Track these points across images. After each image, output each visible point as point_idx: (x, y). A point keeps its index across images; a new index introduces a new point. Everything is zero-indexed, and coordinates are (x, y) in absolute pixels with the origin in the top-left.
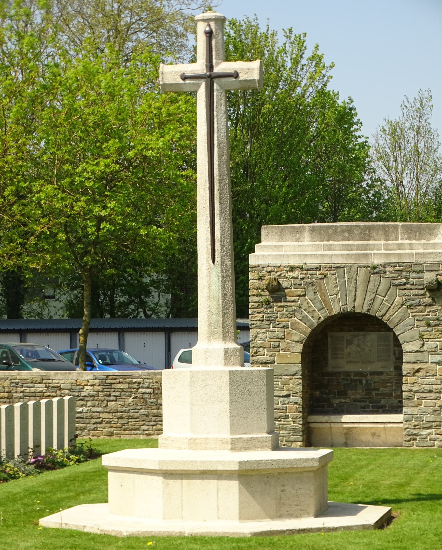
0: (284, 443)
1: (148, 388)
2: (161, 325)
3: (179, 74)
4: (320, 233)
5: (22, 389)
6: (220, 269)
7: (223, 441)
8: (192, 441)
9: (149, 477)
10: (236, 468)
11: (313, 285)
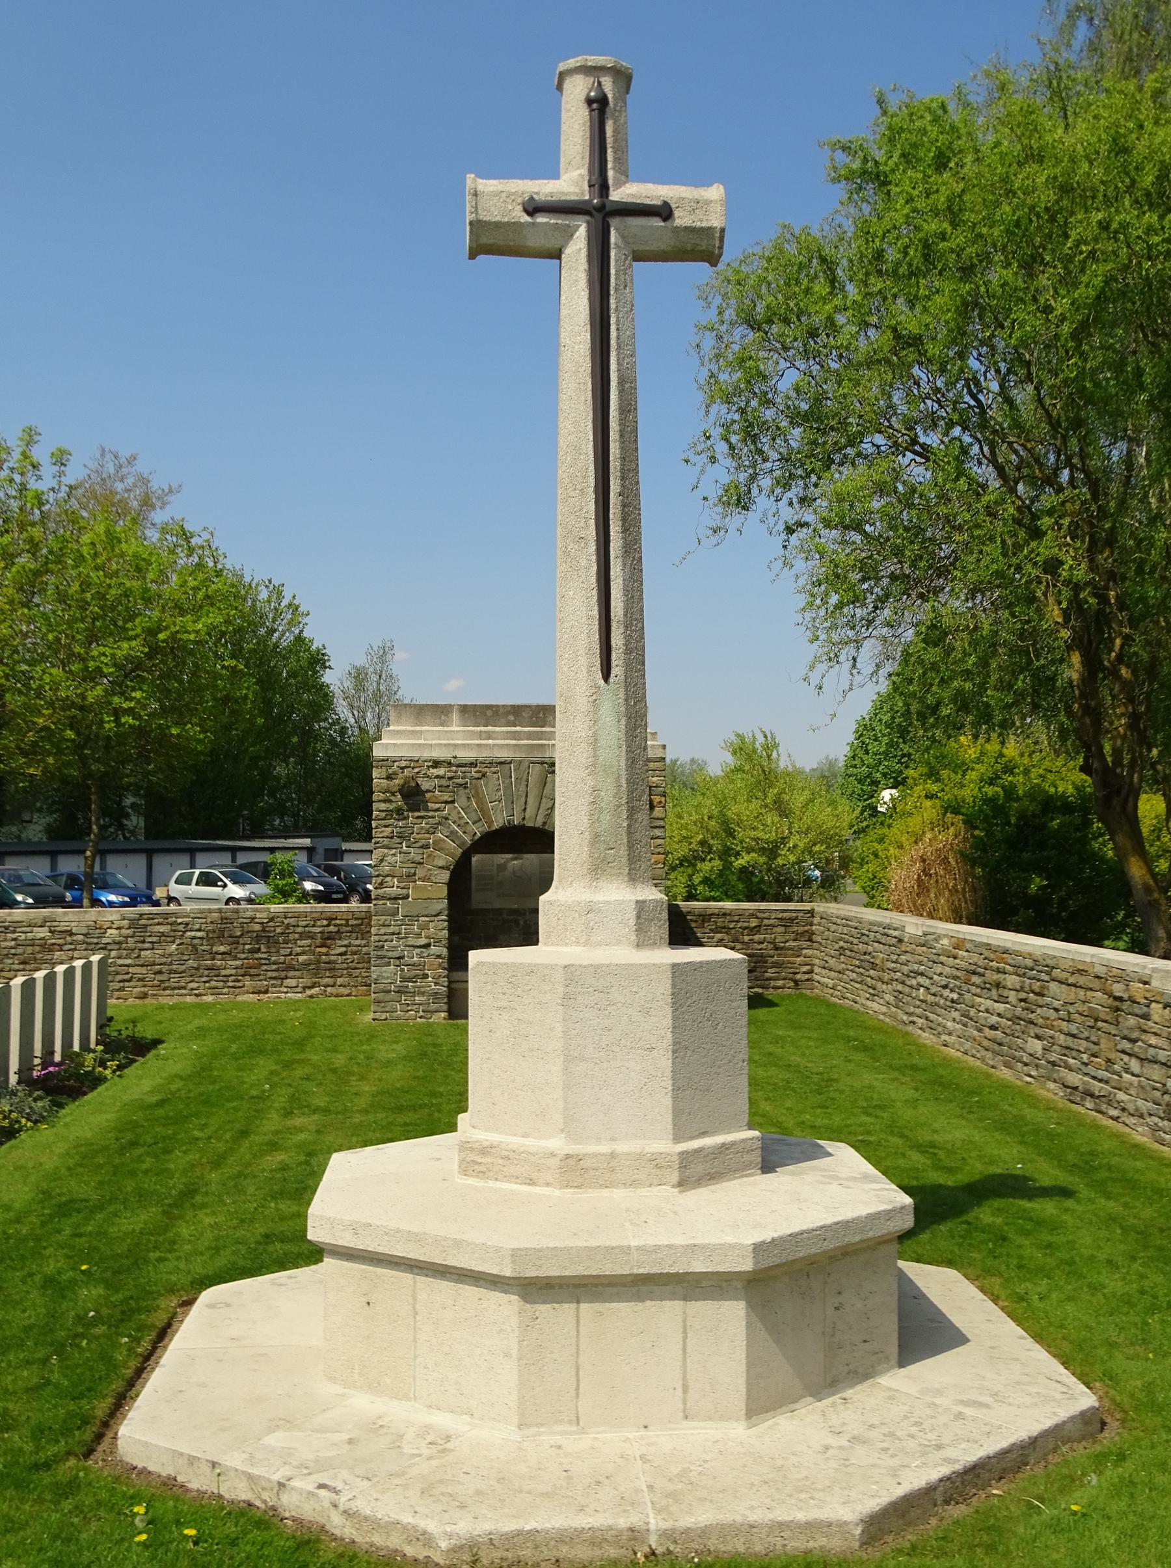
0: (421, 1013)
1: (199, 930)
2: (143, 847)
3: (519, 200)
4: (475, 715)
5: (14, 936)
6: (622, 695)
7: (657, 1162)
8: (571, 1162)
9: (470, 1292)
10: (747, 1265)
11: (466, 788)
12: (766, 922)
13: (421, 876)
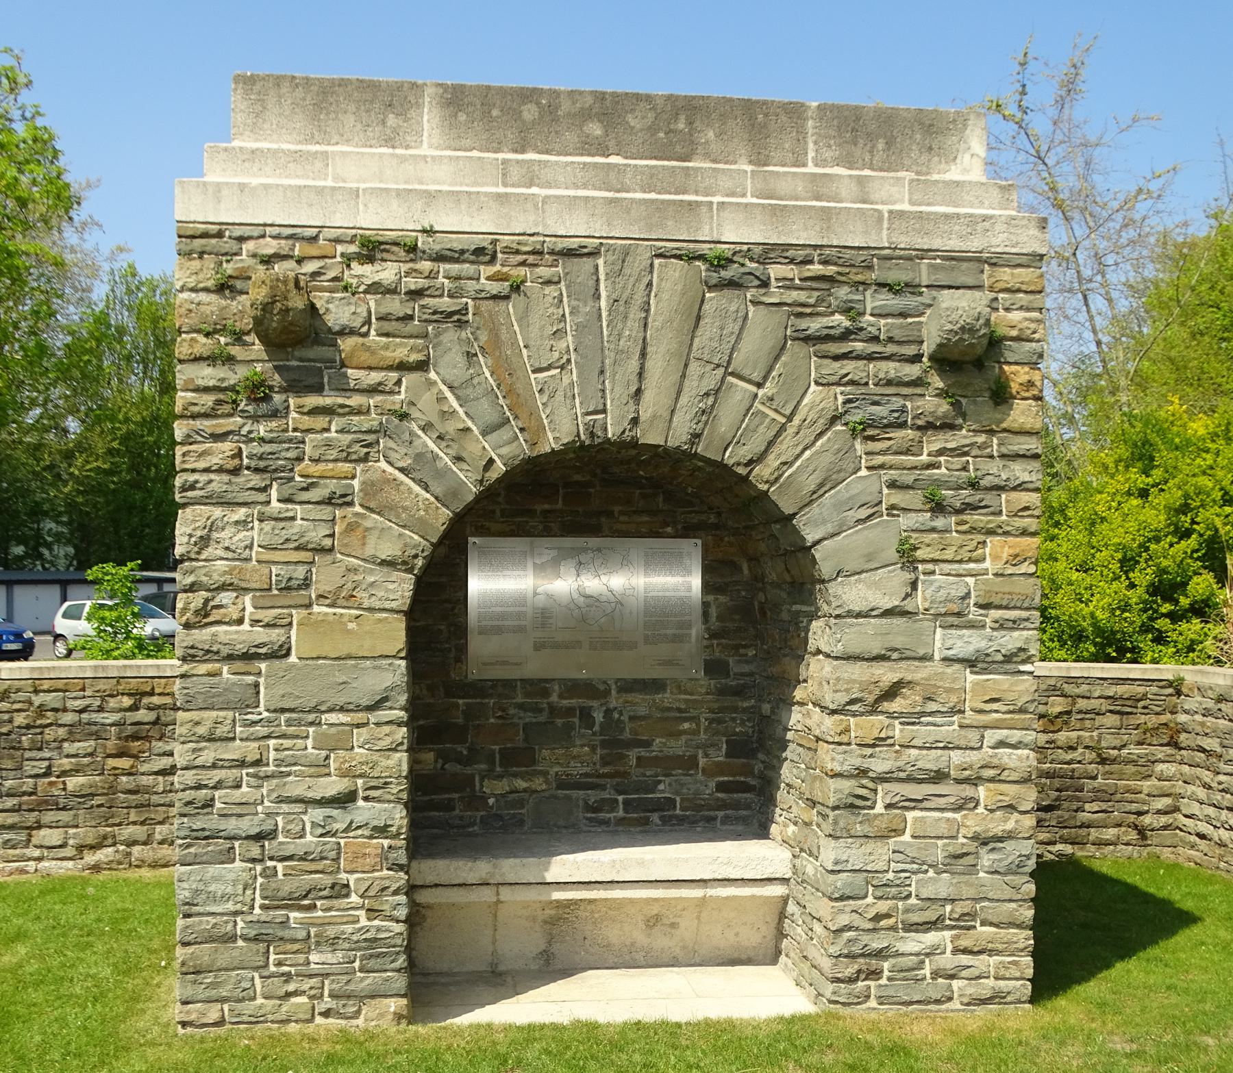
0: (328, 1002)
11: (461, 324)
12: (1082, 704)
13: (324, 588)
